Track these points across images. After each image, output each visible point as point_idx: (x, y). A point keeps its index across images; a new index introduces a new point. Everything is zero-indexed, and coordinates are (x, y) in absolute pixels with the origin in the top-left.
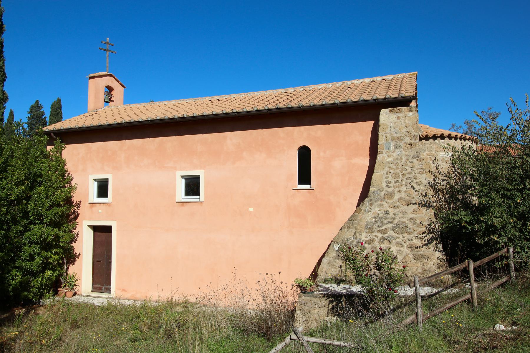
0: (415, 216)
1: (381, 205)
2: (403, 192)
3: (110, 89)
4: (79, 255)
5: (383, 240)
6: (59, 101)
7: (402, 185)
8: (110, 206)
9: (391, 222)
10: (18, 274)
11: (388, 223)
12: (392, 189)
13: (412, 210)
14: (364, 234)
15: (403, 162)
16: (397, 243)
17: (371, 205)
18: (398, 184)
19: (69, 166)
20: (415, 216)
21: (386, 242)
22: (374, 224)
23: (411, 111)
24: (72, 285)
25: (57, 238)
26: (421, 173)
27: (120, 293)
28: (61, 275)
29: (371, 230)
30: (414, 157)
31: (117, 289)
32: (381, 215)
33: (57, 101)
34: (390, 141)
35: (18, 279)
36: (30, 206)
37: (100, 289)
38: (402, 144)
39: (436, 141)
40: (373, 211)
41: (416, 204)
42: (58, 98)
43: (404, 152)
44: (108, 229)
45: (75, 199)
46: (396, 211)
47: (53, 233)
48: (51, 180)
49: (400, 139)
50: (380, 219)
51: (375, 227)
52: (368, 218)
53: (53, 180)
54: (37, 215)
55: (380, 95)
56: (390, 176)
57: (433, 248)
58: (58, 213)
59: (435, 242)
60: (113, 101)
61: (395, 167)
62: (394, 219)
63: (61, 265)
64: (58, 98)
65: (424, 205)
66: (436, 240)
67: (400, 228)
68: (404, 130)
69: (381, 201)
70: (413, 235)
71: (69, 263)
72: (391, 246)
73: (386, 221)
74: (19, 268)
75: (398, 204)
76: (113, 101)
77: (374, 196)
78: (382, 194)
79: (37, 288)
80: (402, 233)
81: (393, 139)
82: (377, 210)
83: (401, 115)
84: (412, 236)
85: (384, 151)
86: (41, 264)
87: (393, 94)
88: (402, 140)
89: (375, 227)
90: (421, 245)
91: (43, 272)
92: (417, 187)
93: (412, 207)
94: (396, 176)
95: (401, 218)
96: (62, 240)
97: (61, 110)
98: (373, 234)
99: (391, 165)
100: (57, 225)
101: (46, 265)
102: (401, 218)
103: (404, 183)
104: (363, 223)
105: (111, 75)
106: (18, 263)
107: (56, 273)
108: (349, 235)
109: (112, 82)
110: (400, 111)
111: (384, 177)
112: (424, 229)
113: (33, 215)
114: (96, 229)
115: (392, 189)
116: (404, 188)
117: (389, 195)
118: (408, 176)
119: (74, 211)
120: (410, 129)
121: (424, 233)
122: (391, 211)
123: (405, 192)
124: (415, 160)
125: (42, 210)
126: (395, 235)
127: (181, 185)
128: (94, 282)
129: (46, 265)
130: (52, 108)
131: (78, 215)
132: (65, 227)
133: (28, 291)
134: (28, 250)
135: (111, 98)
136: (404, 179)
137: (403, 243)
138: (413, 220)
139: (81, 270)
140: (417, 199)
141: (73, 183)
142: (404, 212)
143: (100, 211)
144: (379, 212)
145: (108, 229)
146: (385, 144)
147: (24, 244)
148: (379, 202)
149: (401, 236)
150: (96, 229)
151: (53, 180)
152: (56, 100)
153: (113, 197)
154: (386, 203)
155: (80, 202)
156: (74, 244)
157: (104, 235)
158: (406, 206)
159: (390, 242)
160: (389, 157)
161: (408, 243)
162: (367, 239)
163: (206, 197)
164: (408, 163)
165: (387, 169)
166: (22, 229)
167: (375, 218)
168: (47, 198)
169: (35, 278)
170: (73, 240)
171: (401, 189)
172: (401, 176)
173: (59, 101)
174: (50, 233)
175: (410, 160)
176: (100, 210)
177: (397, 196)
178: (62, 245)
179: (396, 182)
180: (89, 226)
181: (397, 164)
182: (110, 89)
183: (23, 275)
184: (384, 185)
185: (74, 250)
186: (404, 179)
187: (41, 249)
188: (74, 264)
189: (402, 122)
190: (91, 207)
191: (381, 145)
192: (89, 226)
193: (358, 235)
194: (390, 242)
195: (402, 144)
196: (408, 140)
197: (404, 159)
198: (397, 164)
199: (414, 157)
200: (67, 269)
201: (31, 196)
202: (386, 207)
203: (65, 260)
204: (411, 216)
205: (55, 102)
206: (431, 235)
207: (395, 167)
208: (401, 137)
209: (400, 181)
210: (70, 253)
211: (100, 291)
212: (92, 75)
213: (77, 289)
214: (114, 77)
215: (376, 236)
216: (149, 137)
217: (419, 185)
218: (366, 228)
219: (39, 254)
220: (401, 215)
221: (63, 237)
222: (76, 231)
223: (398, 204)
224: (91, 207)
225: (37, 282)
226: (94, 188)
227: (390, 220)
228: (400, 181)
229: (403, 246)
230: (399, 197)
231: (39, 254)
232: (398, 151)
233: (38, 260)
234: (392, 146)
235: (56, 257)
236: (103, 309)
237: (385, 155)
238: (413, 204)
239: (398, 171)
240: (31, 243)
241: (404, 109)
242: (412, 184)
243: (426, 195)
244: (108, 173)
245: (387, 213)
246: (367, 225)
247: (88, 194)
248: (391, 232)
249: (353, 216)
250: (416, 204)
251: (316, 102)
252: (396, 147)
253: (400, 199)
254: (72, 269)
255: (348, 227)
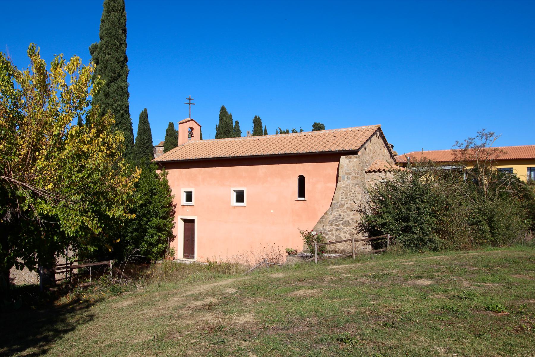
0: (354, 217)
1: (337, 211)
2: (349, 204)
3: (192, 129)
4: (176, 236)
5: (337, 230)
6: (146, 110)
7: (348, 200)
8: (193, 207)
9: (342, 220)
10: (146, 245)
11: (340, 221)
12: (344, 202)
13: (352, 214)
14: (328, 227)
15: (350, 187)
16: (344, 232)
17: (332, 210)
18: (347, 199)
19: (170, 183)
20: (354, 217)
21: (338, 231)
22: (333, 221)
23: (356, 158)
24: (173, 254)
25: (165, 225)
26: (359, 193)
27: (199, 258)
28: (166, 247)
29: (331, 224)
30: (356, 184)
31: (198, 256)
32: (337, 216)
33: (144, 111)
34: (344, 175)
35: (145, 248)
36: (151, 207)
37: (188, 256)
38: (350, 177)
39: (376, 174)
40: (333, 214)
41: (355, 211)
42: (145, 108)
43: (351, 182)
44: (192, 221)
45: (174, 203)
46: (345, 214)
47: (163, 222)
48: (162, 193)
49: (350, 174)
50: (336, 219)
51: (334, 223)
52: (330, 218)
53: (163, 193)
54: (155, 212)
55: (340, 149)
56: (343, 194)
57: (361, 235)
58: (165, 211)
59: (362, 231)
60: (194, 137)
61: (346, 190)
62: (343, 218)
63: (167, 241)
64: (145, 108)
65: (359, 212)
66: (363, 230)
67: (346, 224)
68: (352, 169)
69: (337, 209)
70: (351, 228)
71: (170, 241)
72: (341, 233)
73: (339, 220)
74: (147, 242)
75: (346, 210)
76: (194, 137)
77: (334, 206)
78: (339, 204)
79: (155, 253)
80: (347, 226)
81: (346, 174)
82: (335, 213)
83: (351, 160)
84: (351, 228)
85: (342, 180)
86: (157, 240)
87: (347, 148)
88: (350, 174)
89: (334, 223)
90: (356, 233)
91: (158, 244)
92: (356, 201)
93: (353, 212)
94: (346, 194)
95: (347, 218)
96: (168, 227)
97: (147, 119)
98: (332, 227)
99: (344, 189)
100: (164, 218)
101: (159, 241)
102: (347, 218)
103: (350, 199)
104: (328, 221)
105: (192, 120)
106: (146, 239)
107: (164, 246)
108: (320, 227)
109: (193, 124)
110: (351, 158)
111: (340, 195)
112: (357, 224)
113: (153, 212)
114: (185, 221)
115: (344, 202)
116: (349, 202)
117: (342, 205)
118: (352, 195)
119: (173, 210)
120: (355, 168)
121: (357, 227)
122: (342, 214)
123: (350, 204)
124: (356, 186)
125: (157, 209)
126: (343, 227)
127: (234, 196)
128: (184, 253)
129: (159, 241)
130: (140, 118)
131: (175, 212)
132: (168, 219)
133: (151, 255)
134: (150, 231)
135: (192, 135)
136: (350, 196)
137: (347, 232)
138: (353, 219)
139: (177, 245)
140: (356, 208)
141: (172, 194)
142: (348, 215)
143: (188, 210)
144: (336, 215)
145: (192, 221)
146: (342, 176)
147: (148, 229)
148: (337, 209)
149: (346, 228)
150: (185, 221)
151: (163, 193)
152: (143, 110)
153: (195, 203)
154: (340, 209)
155: (176, 204)
156: (173, 230)
157: (190, 224)
158: (350, 212)
159: (340, 231)
160: (344, 184)
161: (349, 232)
162: (329, 229)
163: (247, 203)
164: (353, 188)
165: (342, 191)
166: (147, 220)
167: (334, 218)
168: (160, 202)
169: (154, 248)
170: (173, 227)
171: (348, 202)
172: (348, 195)
173: (146, 110)
174: (162, 222)
175: (354, 186)
176: (188, 209)
177: (346, 206)
178: (107, 244)
179: (346, 198)
180: (181, 219)
181: (347, 188)
182: (192, 129)
183: (148, 246)
184: (340, 199)
185: (173, 233)
186: (350, 196)
187: (157, 231)
188: (173, 241)
189: (351, 164)
190: (183, 208)
191: (340, 176)
192: (181, 219)
193: (325, 227)
194: (340, 231)
195: (350, 177)
196: (353, 174)
197: (351, 185)
198: (347, 188)
199: (356, 184)
200: (170, 244)
201: (151, 201)
202: (340, 212)
203: (169, 238)
204: (352, 217)
205: (142, 112)
206: (360, 228)
207: (346, 190)
208: (350, 172)
209: (348, 198)
210: (171, 235)
211: (188, 257)
212: (181, 122)
213: (175, 256)
214: (194, 121)
215: (334, 228)
216: (215, 167)
217: (357, 200)
218: (329, 223)
219: (156, 234)
220: (347, 217)
221: (168, 225)
222: (174, 222)
223: (346, 210)
224: (183, 208)
225: (155, 250)
226: (184, 196)
227: (341, 219)
228: (348, 198)
229: (346, 233)
230: (347, 207)
231: (156, 234)
232: (349, 181)
233: (156, 238)
234: (345, 178)
235: (164, 237)
236: (191, 265)
237: (342, 182)
238: (354, 211)
239: (348, 192)
240: (151, 227)
241: (353, 156)
242: (354, 200)
243: (360, 206)
244: (192, 187)
245: (340, 215)
246: (329, 222)
247: (180, 200)
248: (341, 226)
249: (323, 216)
250: (355, 211)
251: (307, 151)
252: (348, 178)
253: (347, 207)
254: (172, 244)
255: (320, 223)
